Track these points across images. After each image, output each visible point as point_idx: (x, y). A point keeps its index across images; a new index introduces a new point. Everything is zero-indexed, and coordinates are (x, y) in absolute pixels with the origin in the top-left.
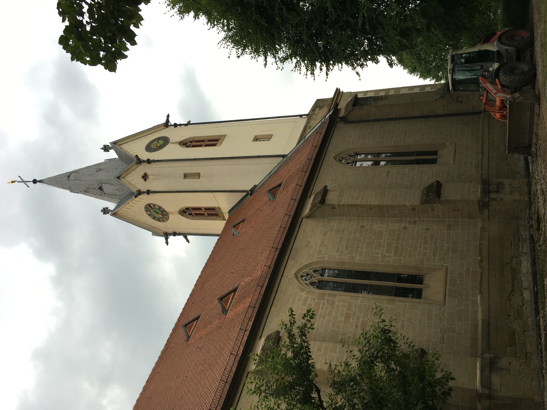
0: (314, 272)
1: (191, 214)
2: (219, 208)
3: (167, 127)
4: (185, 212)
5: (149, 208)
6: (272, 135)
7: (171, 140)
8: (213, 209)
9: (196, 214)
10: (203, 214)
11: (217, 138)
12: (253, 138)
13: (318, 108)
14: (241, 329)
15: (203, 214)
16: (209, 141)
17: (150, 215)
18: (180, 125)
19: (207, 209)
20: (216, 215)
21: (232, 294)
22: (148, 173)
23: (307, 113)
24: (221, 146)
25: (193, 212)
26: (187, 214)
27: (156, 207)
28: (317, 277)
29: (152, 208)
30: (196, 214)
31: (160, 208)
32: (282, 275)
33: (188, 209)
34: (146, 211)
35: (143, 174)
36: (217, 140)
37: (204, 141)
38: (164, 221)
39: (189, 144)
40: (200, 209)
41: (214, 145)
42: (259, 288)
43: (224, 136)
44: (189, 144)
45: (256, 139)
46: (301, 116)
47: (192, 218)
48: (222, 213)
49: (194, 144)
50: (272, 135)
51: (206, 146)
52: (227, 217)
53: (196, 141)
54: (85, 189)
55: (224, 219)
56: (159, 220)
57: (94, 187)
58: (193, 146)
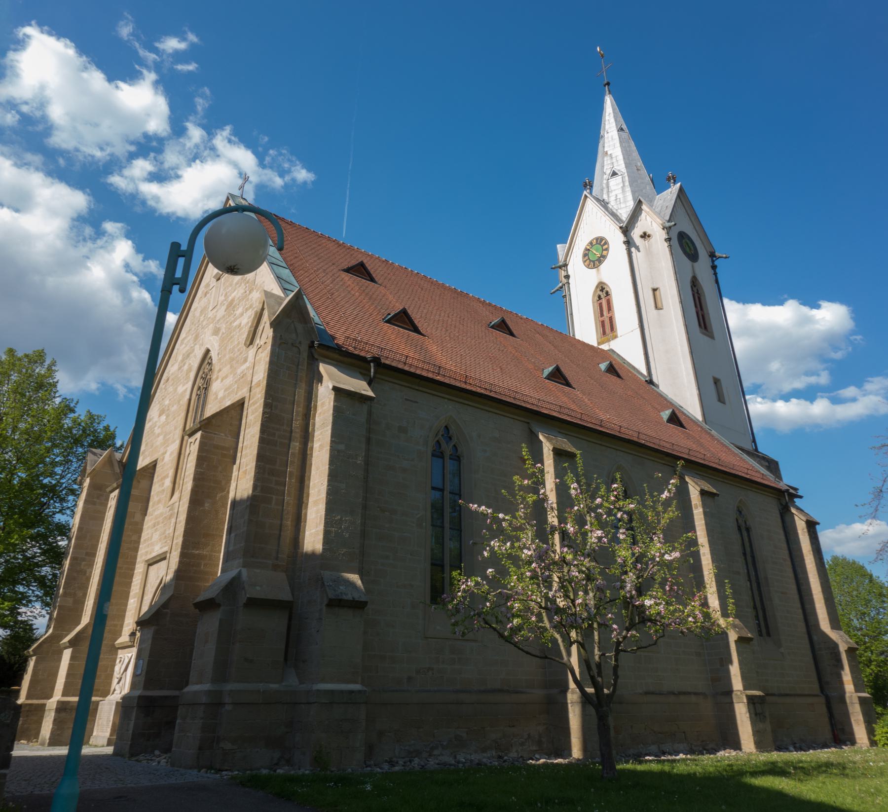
0: (454, 446)
1: (600, 298)
6: (724, 403)
7: (696, 264)
9: (601, 306)
10: (602, 315)
11: (708, 327)
12: (717, 376)
13: (767, 464)
15: (602, 315)
16: (703, 316)
17: (591, 243)
18: (715, 274)
19: (611, 319)
20: (604, 333)
22: (652, 240)
23: (759, 450)
25: (604, 301)
26: (601, 293)
27: (605, 253)
28: (448, 450)
29: (602, 246)
30: (601, 306)
31: (604, 257)
33: (607, 294)
34: (597, 239)
35: (649, 232)
36: (706, 328)
37: (702, 309)
38: (584, 262)
40: (610, 308)
41: (700, 325)
42: (558, 409)
44: (695, 289)
45: (716, 381)
46: (754, 441)
48: (609, 341)
50: (724, 403)
51: (697, 313)
52: (605, 347)
55: (599, 344)
57: (615, 164)
58: (693, 295)
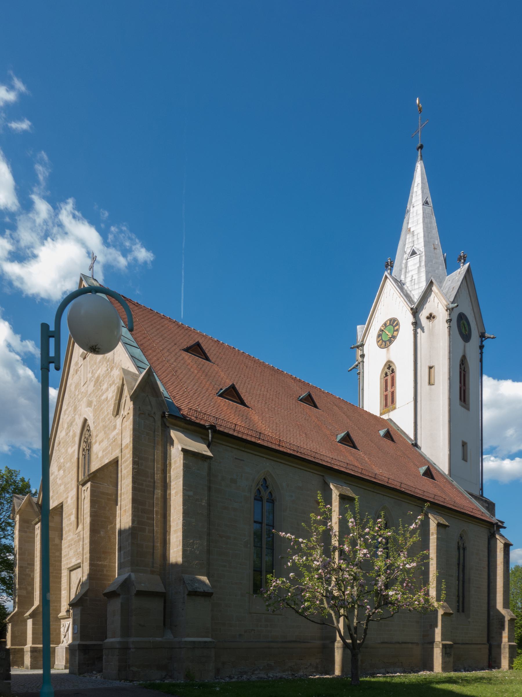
0: (270, 492)
1: (386, 375)
2: (395, 408)
3: (480, 336)
4: (389, 368)
5: (393, 324)
6: (466, 461)
7: (468, 344)
8: (393, 401)
9: (386, 382)
10: (386, 390)
12: (465, 440)
13: (487, 505)
14: (260, 433)
15: (386, 390)
17: (385, 324)
19: (393, 393)
20: (386, 405)
21: (352, 445)
22: (436, 321)
23: (484, 495)
24: (460, 407)
25: (389, 378)
27: (396, 333)
28: (265, 495)
32: (384, 495)
33: (393, 371)
34: (390, 320)
36: (464, 401)
38: (378, 342)
39: (463, 367)
40: (393, 384)
42: (345, 465)
43: (468, 409)
44: (463, 367)
45: (464, 444)
46: (482, 489)
47: (383, 377)
48: (389, 412)
49: (463, 372)
51: (460, 388)
52: (385, 417)
53: (464, 375)
54: (412, 230)
55: (381, 414)
56: (379, 335)
57: (416, 243)
